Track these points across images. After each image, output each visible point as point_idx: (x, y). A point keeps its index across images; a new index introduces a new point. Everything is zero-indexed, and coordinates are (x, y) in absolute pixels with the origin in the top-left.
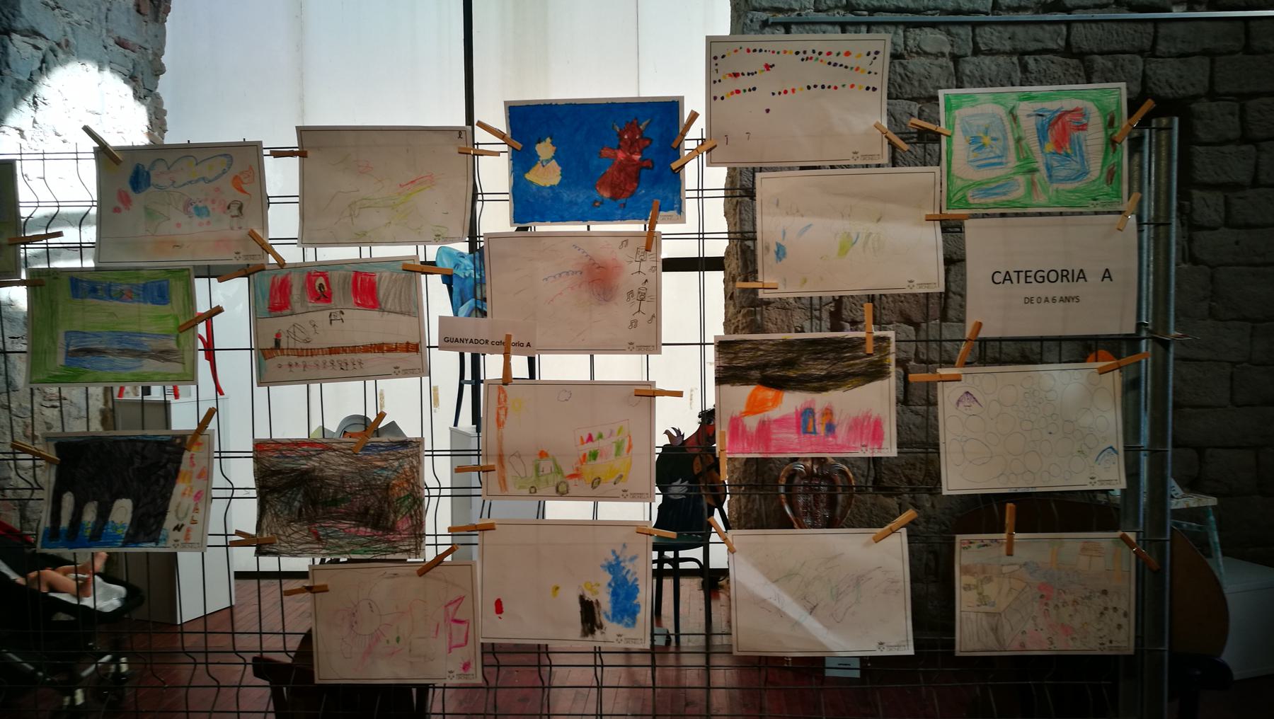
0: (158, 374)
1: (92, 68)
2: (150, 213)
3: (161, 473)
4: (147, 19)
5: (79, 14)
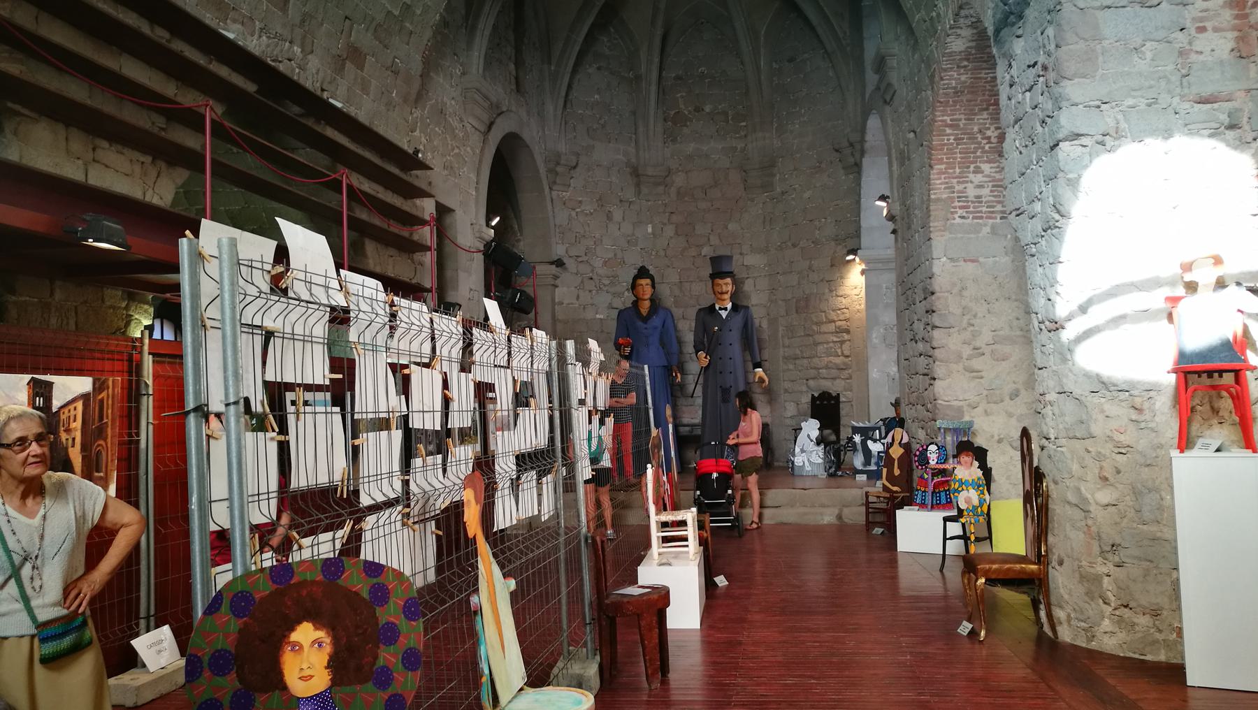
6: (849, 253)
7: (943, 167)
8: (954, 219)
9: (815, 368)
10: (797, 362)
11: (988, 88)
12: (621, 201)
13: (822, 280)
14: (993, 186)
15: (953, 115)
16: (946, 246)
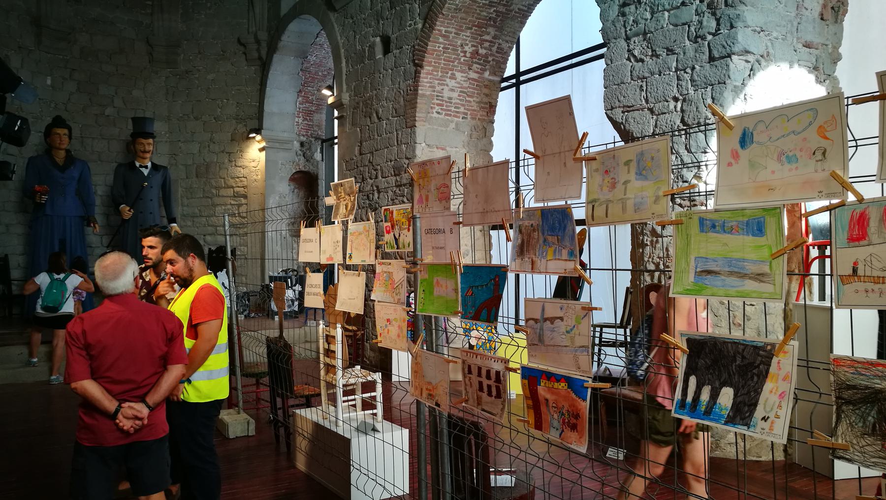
0: (755, 292)
1: (785, 66)
2: (752, 165)
3: (755, 371)
4: (828, 22)
5: (777, 32)
6: (252, 131)
7: (431, 68)
8: (433, 113)
9: (212, 226)
10: (195, 219)
11: (478, 11)
12: (20, 47)
13: (223, 152)
14: (461, 92)
15: (448, 27)
16: (426, 134)
